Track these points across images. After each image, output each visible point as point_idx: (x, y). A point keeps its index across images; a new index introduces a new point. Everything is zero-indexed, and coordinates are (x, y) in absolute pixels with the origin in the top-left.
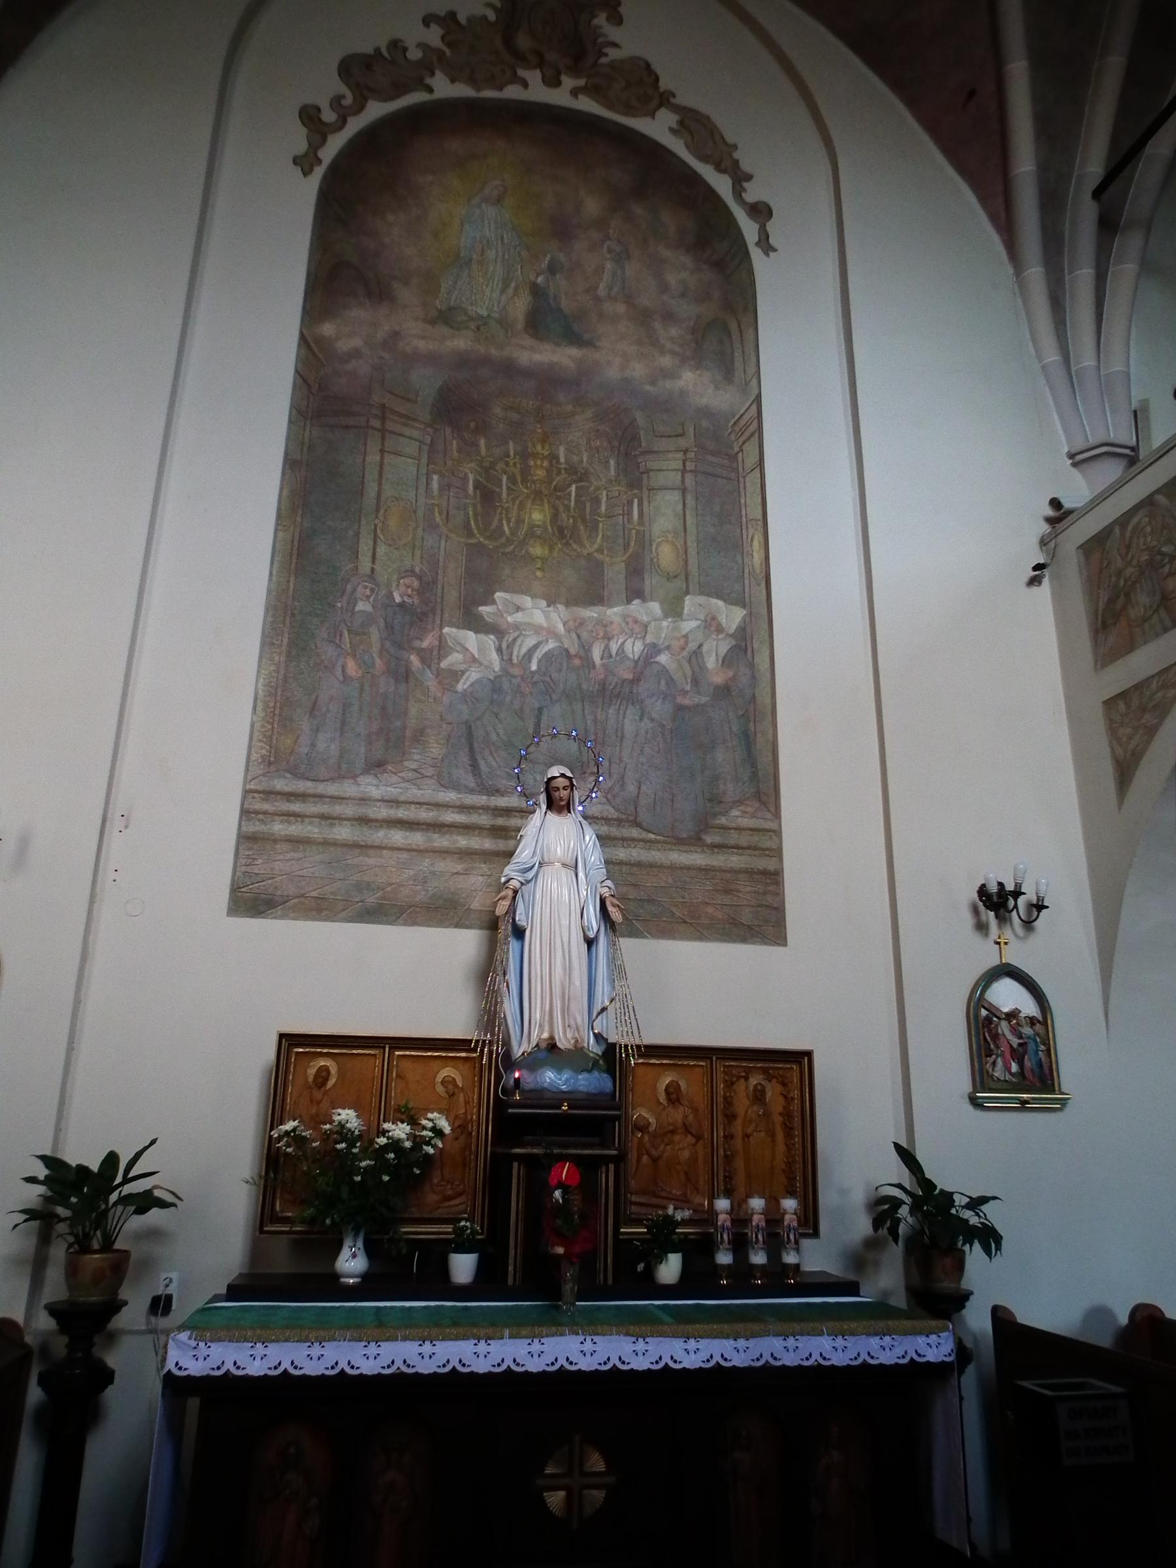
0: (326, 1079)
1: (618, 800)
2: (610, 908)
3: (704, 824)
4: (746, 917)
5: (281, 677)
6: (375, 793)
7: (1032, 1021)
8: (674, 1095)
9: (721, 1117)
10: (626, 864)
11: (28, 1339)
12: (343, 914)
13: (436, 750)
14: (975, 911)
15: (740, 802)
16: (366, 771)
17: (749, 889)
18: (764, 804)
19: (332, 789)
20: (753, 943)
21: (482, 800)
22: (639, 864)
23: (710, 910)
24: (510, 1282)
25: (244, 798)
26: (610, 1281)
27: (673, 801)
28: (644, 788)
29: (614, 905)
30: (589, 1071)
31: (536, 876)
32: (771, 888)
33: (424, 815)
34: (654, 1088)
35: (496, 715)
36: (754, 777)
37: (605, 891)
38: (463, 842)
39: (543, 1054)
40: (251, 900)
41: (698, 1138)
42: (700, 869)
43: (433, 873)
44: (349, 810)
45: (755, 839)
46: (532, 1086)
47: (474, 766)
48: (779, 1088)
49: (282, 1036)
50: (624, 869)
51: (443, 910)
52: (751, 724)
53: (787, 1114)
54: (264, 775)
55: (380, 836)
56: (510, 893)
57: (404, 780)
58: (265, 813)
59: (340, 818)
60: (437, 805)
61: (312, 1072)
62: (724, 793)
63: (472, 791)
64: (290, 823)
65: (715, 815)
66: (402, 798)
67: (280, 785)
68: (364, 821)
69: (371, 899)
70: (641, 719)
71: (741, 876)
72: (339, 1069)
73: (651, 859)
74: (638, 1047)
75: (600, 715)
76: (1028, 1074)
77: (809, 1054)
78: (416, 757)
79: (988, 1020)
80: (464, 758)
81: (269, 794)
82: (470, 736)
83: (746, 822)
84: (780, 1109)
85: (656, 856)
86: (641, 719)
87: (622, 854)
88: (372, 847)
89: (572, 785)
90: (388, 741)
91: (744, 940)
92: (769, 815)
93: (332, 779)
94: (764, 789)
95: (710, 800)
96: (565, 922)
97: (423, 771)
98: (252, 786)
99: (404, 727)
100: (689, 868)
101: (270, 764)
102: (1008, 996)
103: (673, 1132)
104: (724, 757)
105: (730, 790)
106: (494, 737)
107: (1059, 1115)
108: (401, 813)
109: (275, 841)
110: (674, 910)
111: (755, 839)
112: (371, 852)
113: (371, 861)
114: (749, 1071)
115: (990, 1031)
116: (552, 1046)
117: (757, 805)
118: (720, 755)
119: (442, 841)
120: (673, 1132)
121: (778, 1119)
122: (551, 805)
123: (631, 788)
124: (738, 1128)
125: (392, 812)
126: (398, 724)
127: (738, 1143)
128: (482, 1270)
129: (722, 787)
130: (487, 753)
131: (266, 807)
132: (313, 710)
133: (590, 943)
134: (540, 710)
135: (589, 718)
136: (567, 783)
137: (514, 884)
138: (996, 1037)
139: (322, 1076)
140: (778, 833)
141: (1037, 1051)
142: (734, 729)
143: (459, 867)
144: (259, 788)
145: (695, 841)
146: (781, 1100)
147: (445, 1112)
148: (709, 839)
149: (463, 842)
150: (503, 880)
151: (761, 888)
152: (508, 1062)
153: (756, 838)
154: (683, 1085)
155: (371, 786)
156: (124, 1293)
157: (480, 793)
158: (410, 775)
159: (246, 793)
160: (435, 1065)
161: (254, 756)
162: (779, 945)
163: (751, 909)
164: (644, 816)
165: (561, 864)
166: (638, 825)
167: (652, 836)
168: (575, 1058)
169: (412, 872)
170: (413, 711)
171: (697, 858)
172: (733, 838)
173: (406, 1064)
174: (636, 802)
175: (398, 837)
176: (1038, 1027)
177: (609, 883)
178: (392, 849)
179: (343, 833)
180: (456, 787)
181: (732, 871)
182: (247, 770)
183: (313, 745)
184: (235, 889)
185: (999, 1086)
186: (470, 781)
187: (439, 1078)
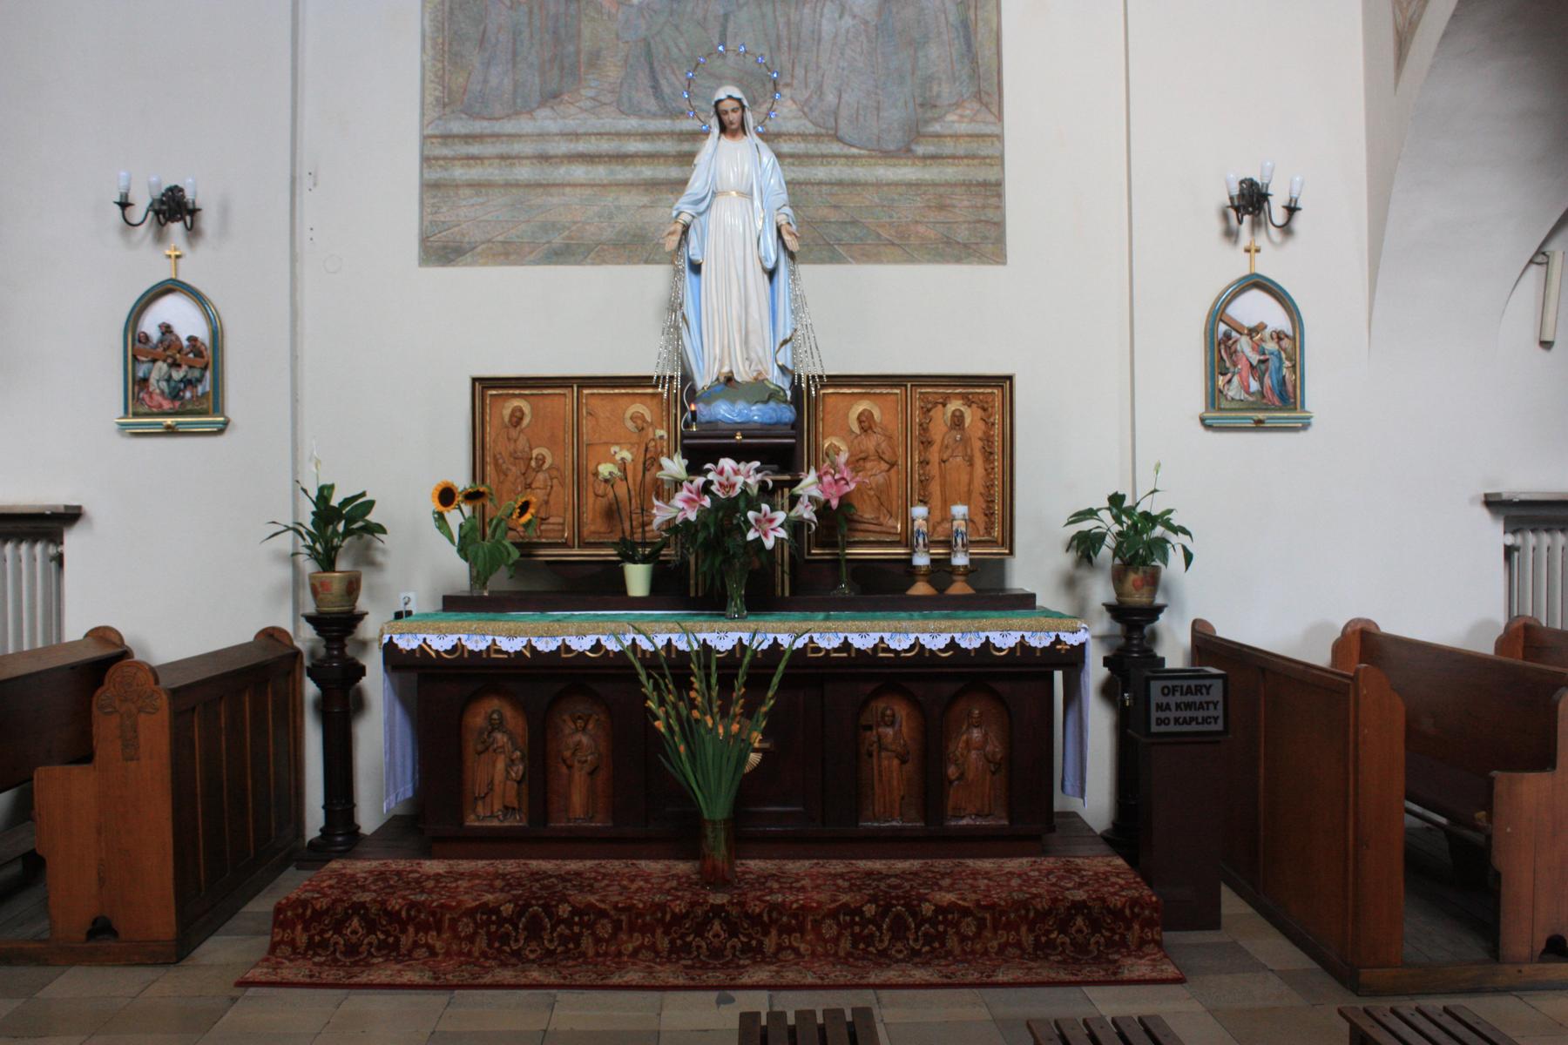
0: (521, 419)
1: (816, 113)
2: (786, 237)
3: (915, 132)
4: (962, 234)
5: (447, 8)
6: (552, 126)
7: (1279, 336)
8: (866, 422)
9: (916, 444)
10: (826, 184)
11: (298, 644)
12: (531, 257)
13: (613, 73)
14: (1225, 216)
15: (958, 105)
16: (543, 103)
17: (966, 203)
18: (987, 106)
19: (508, 127)
20: (970, 263)
21: (665, 124)
22: (840, 183)
23: (921, 229)
24: (692, 594)
25: (423, 145)
26: (787, 593)
27: (878, 109)
28: (845, 97)
29: (791, 234)
30: (766, 402)
31: (709, 207)
32: (992, 201)
33: (606, 146)
34: (846, 416)
35: (677, 27)
36: (975, 75)
37: (782, 219)
38: (647, 172)
39: (719, 388)
40: (441, 250)
41: (892, 465)
42: (910, 185)
43: (618, 208)
44: (528, 148)
45: (974, 146)
46: (707, 418)
47: (656, 87)
48: (980, 413)
49: (474, 380)
50: (824, 188)
51: (633, 246)
52: (972, 12)
53: (988, 439)
54: (440, 118)
55: (561, 173)
56: (679, 228)
57: (583, 110)
58: (445, 158)
59: (518, 157)
60: (618, 135)
61: (507, 412)
62: (939, 96)
63: (655, 116)
64: (469, 166)
65: (927, 122)
66: (581, 131)
67: (457, 127)
68: (544, 158)
69: (558, 240)
70: (841, 17)
71: (958, 190)
72: (533, 409)
73: (854, 177)
74: (820, 377)
75: (794, 17)
76: (1268, 394)
77: (1010, 378)
78: (593, 84)
79: (1227, 336)
80: (643, 79)
81: (446, 138)
82: (649, 53)
83: (963, 128)
84: (980, 434)
85: (860, 172)
86: (841, 17)
87: (801, 173)
88: (554, 185)
89: (743, 107)
90: (562, 68)
91: (958, 260)
92: (991, 118)
93: (508, 116)
94: (983, 84)
95: (922, 105)
96: (739, 253)
97: (602, 99)
98: (429, 131)
99: (578, 52)
100: (896, 184)
101: (445, 106)
102: (1255, 309)
103: (864, 459)
104: (939, 55)
105: (945, 91)
106: (675, 51)
107: (1302, 434)
108: (581, 147)
109: (457, 186)
110: (880, 231)
111: (974, 146)
112: (553, 190)
113: (555, 200)
114: (947, 397)
115: (1228, 348)
116: (729, 379)
117: (976, 106)
118: (934, 51)
119: (625, 173)
120: (864, 459)
121: (978, 445)
122: (724, 129)
123: (831, 98)
124: (934, 455)
125: (572, 146)
126: (571, 48)
127: (934, 469)
128: (656, 583)
129: (935, 88)
130: (668, 71)
131: (445, 152)
132: (482, 41)
133: (771, 274)
134: (726, 16)
135: (781, 20)
136: (736, 105)
137: (685, 218)
138: (1232, 353)
139: (517, 418)
140: (1000, 137)
141: (1280, 369)
142: (952, 18)
143: (645, 200)
144: (437, 132)
145: (905, 152)
146: (982, 425)
147: (631, 446)
148: (920, 150)
149: (647, 172)
150: (675, 213)
151: (979, 202)
152: (692, 395)
153: (975, 145)
154: (877, 414)
155: (546, 121)
156: (362, 604)
157: (664, 116)
158: (589, 104)
159: (425, 138)
160: (623, 401)
161: (429, 99)
162: (998, 263)
163: (970, 226)
164: (845, 129)
165: (739, 191)
166: (837, 138)
167: (855, 151)
168: (760, 391)
169: (596, 209)
170: (586, 33)
171: (907, 172)
172: (949, 147)
173: (595, 402)
174: (836, 114)
175: (579, 172)
176: (1286, 343)
177: (787, 210)
178: (574, 185)
179: (524, 172)
180: (636, 111)
181: (947, 184)
182: (423, 115)
183: (485, 81)
184: (424, 240)
185: (1233, 405)
186: (652, 104)
187: (628, 414)
